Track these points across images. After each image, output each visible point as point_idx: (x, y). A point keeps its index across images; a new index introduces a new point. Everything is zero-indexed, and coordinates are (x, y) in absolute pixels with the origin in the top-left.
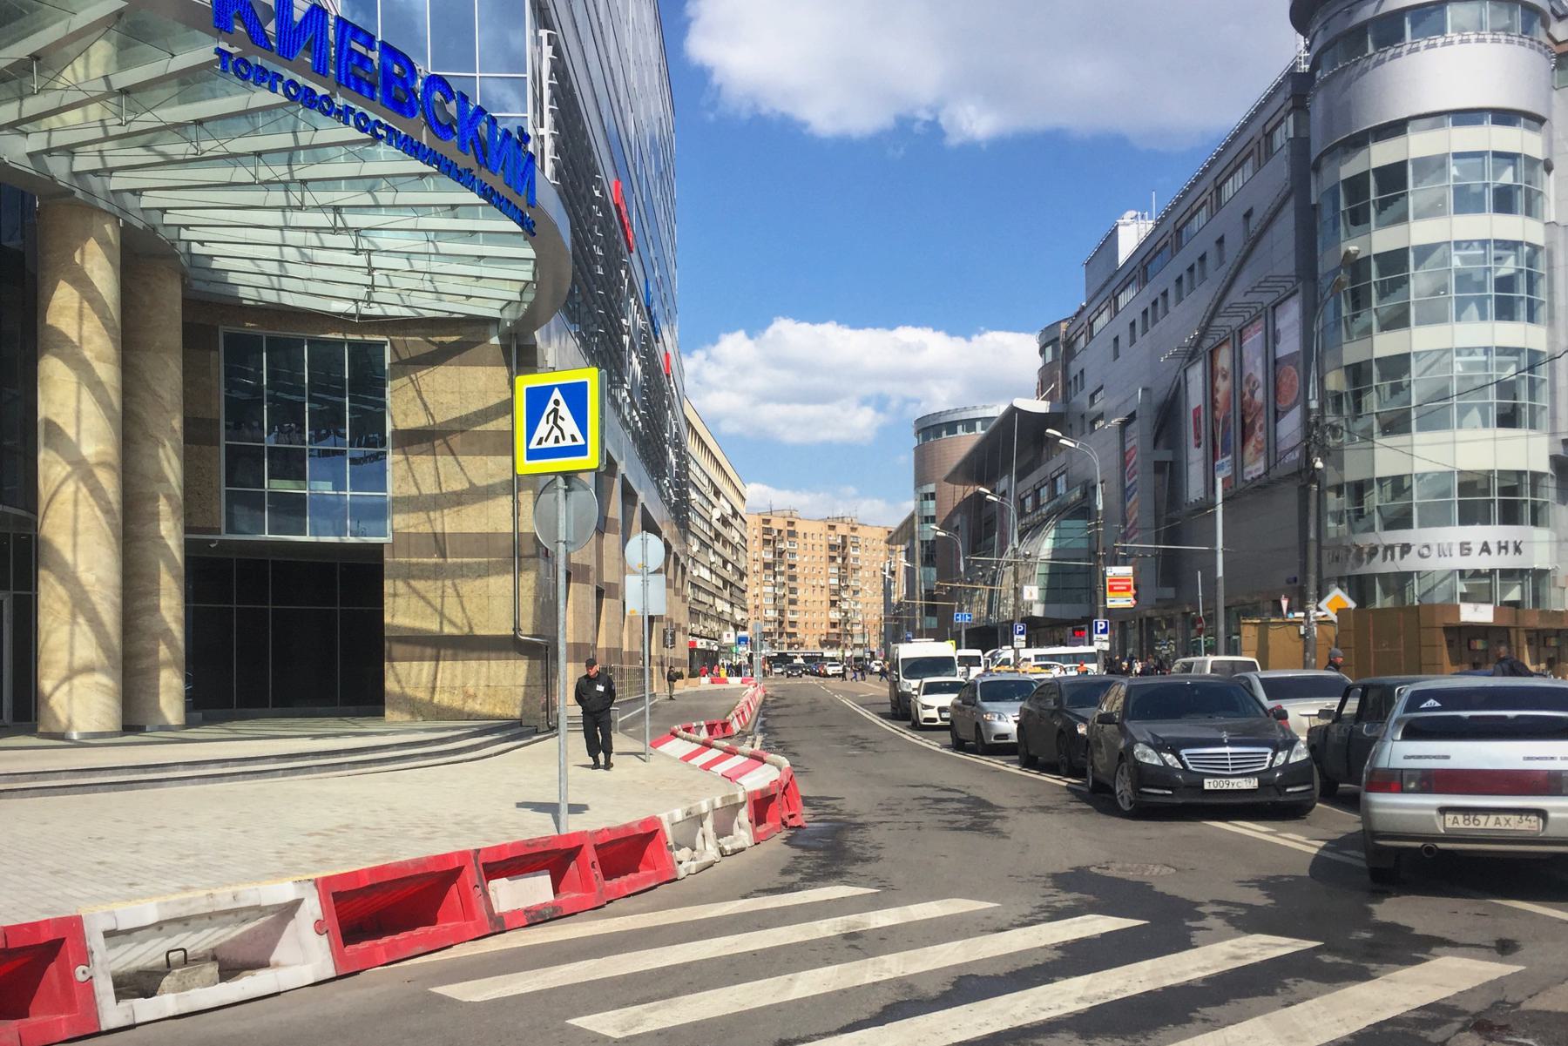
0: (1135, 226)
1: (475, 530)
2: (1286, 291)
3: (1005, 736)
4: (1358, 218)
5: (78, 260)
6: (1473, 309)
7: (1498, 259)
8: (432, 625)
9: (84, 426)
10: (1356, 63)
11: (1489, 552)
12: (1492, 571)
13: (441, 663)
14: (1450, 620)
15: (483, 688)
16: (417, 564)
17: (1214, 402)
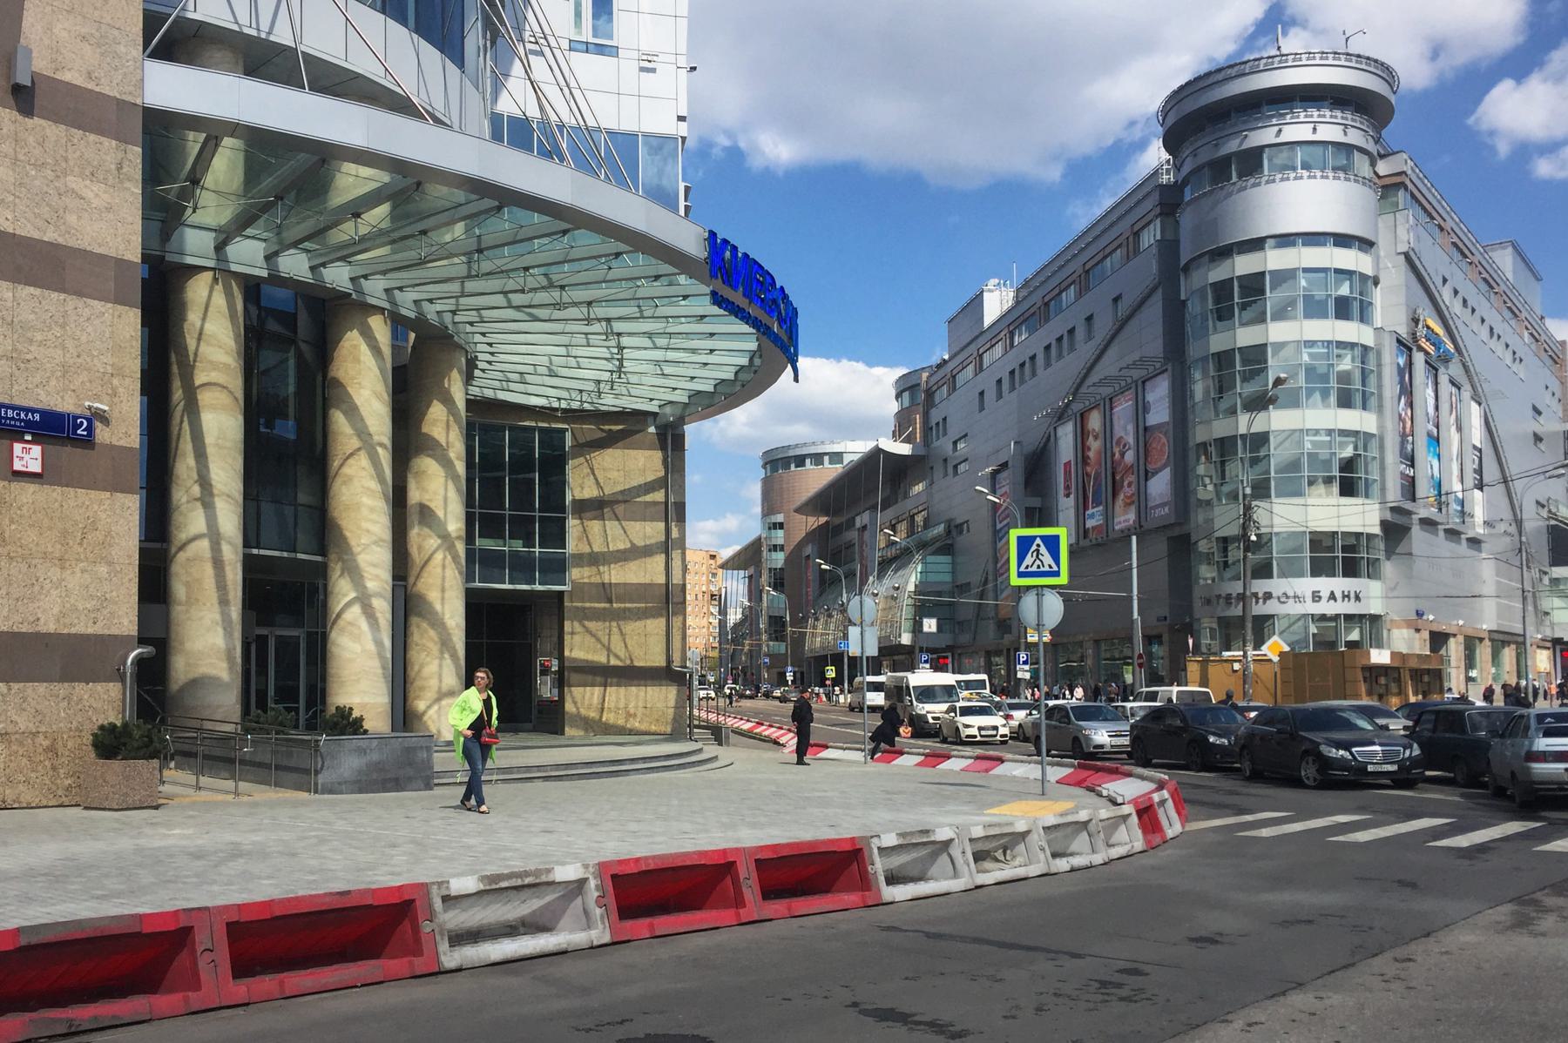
0: (998, 293)
1: (635, 581)
2: (1155, 369)
3: (1102, 746)
4: (1224, 314)
5: (446, 386)
6: (1317, 396)
7: (1339, 356)
8: (601, 658)
9: (449, 509)
10: (1222, 188)
11: (1336, 601)
12: (1337, 616)
13: (608, 688)
14: (1364, 662)
15: (641, 710)
16: (590, 608)
17: (1085, 460)
